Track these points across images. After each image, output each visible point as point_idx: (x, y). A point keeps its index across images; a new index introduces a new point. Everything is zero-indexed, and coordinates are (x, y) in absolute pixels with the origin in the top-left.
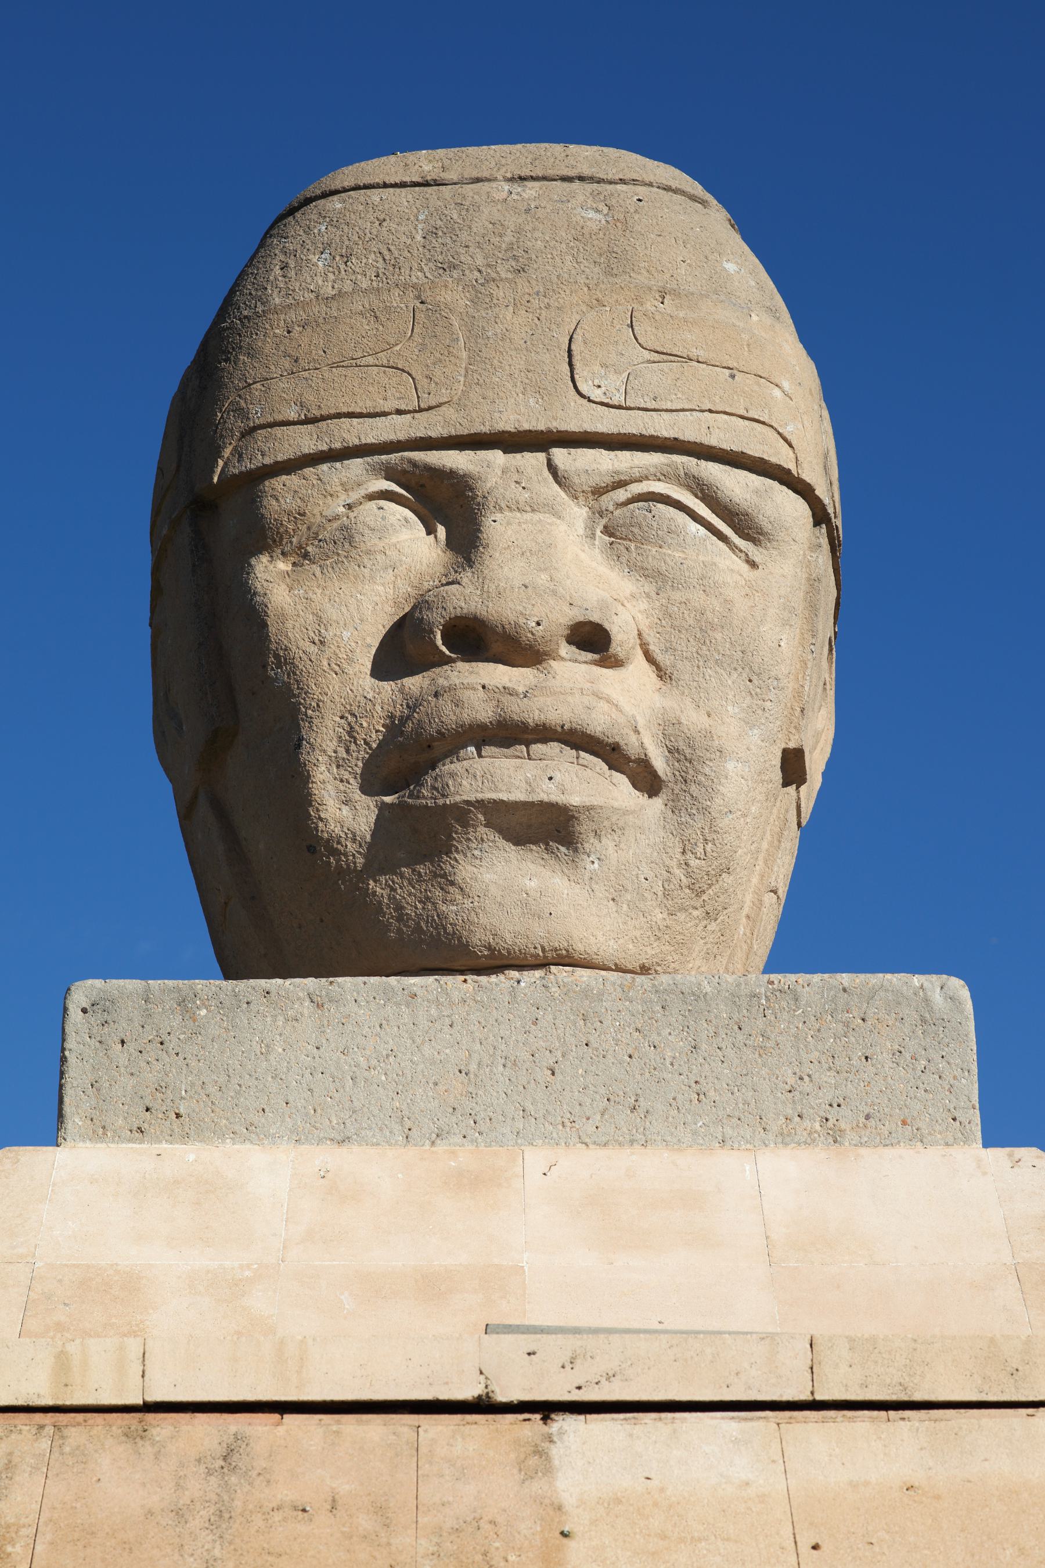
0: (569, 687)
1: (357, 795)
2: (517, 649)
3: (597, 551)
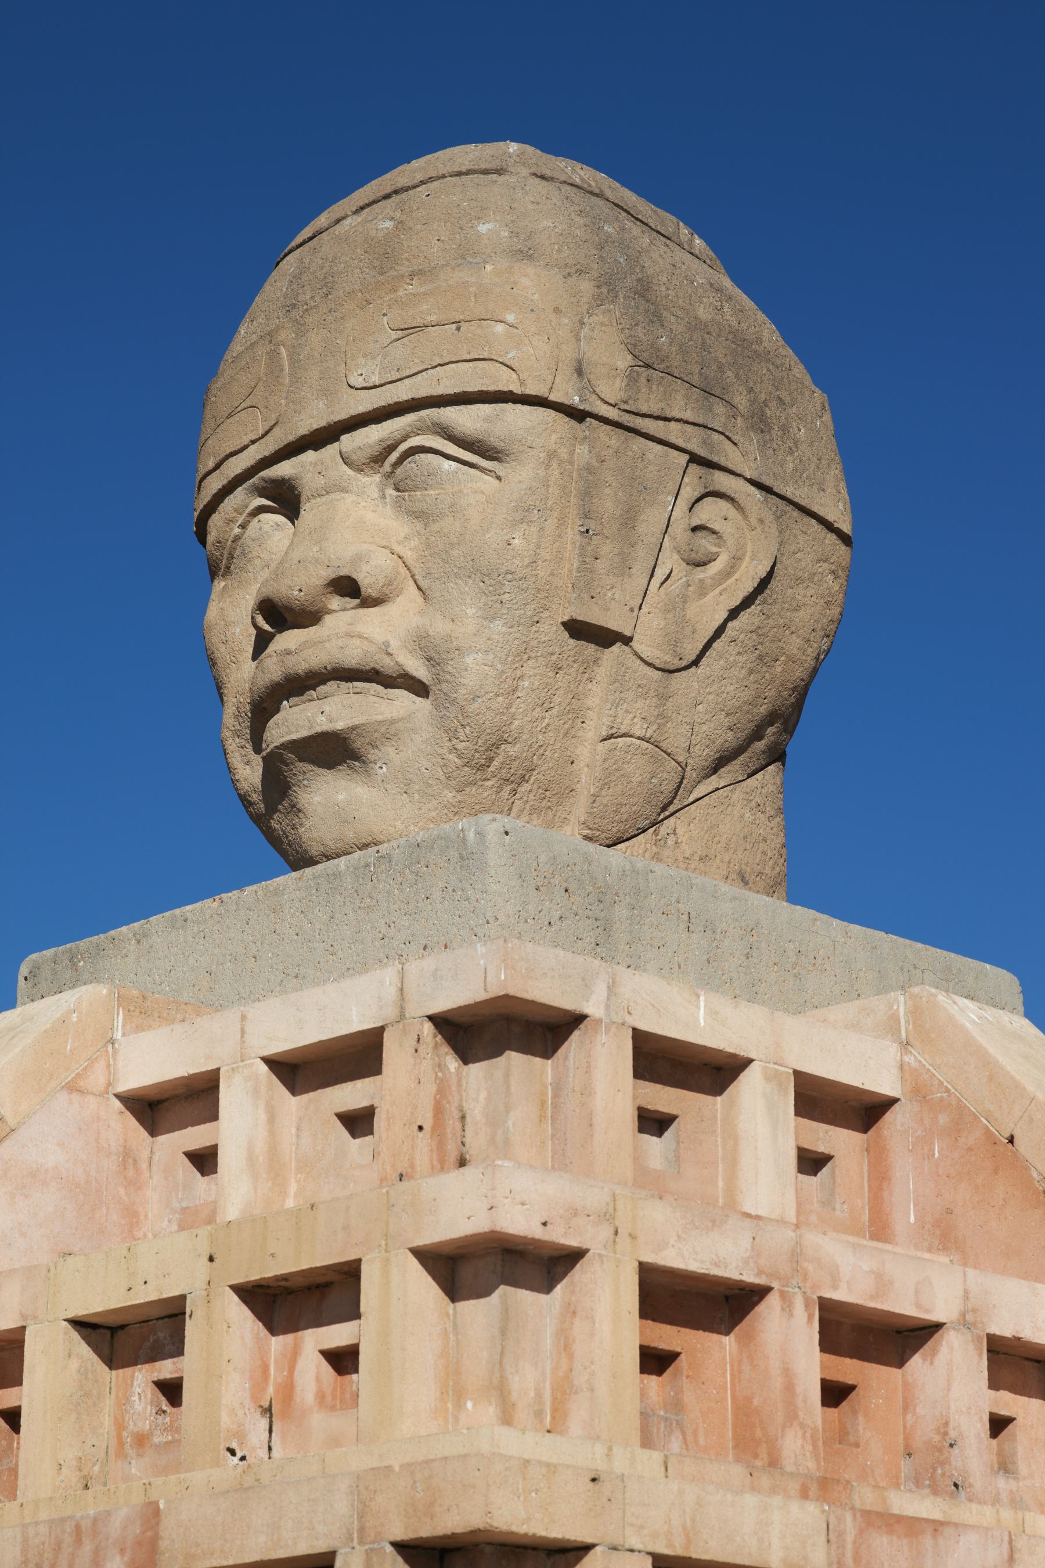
3: (389, 507)
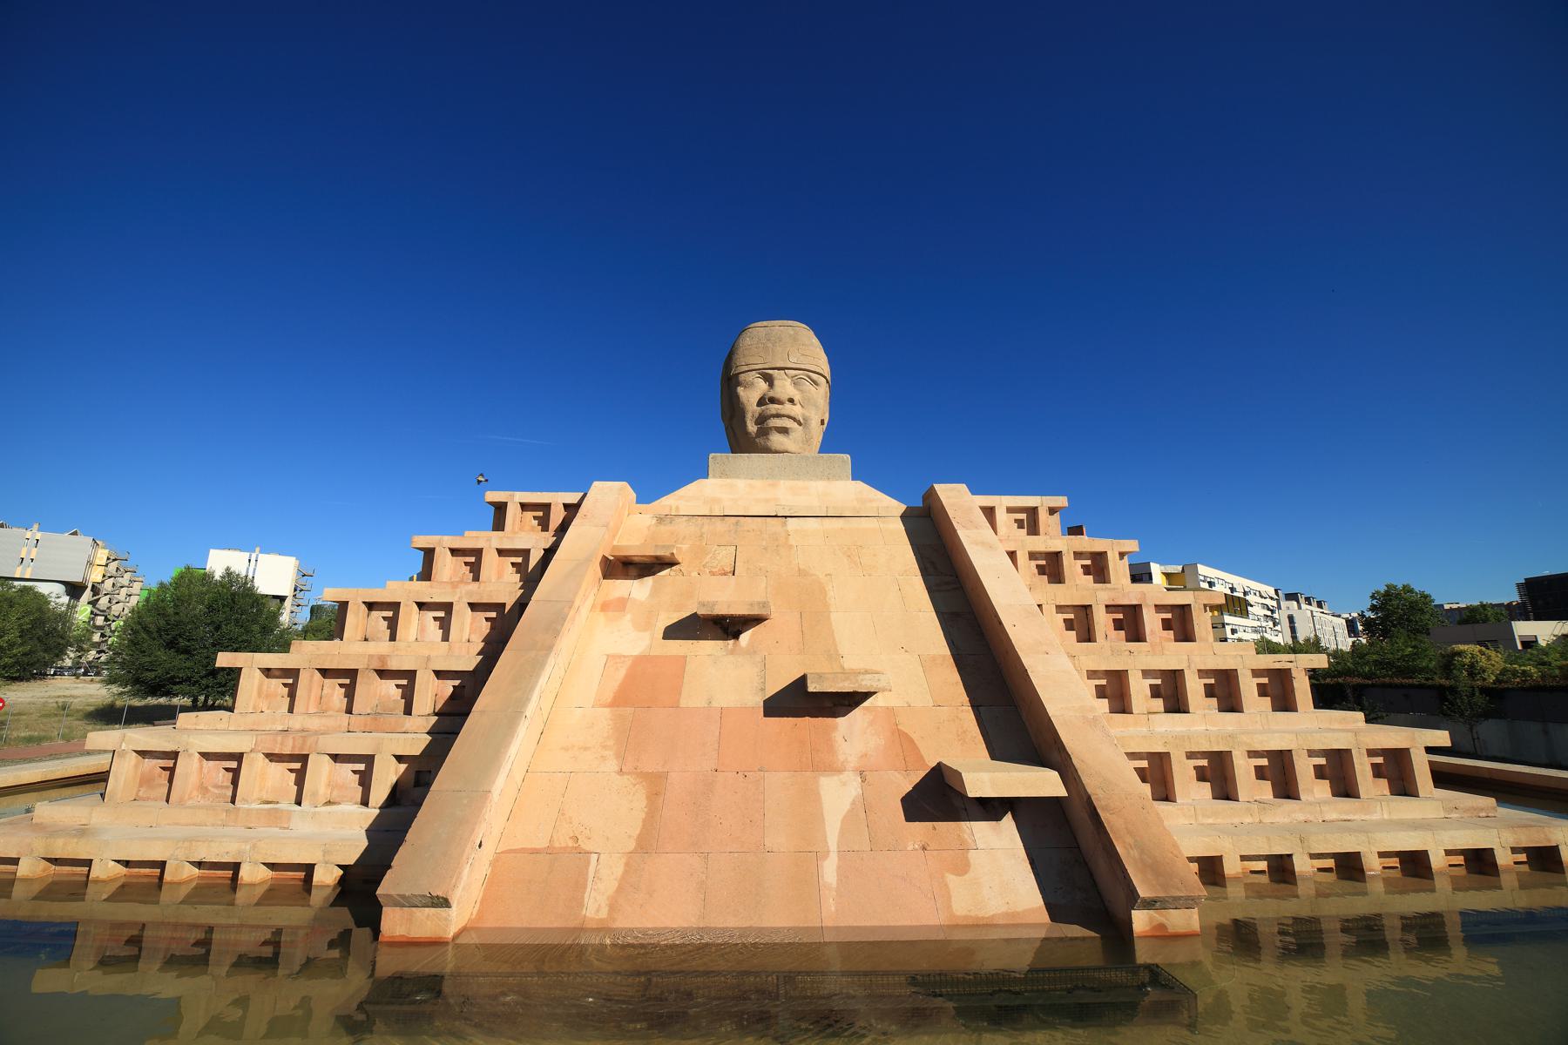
0: (787, 408)
2: (779, 402)
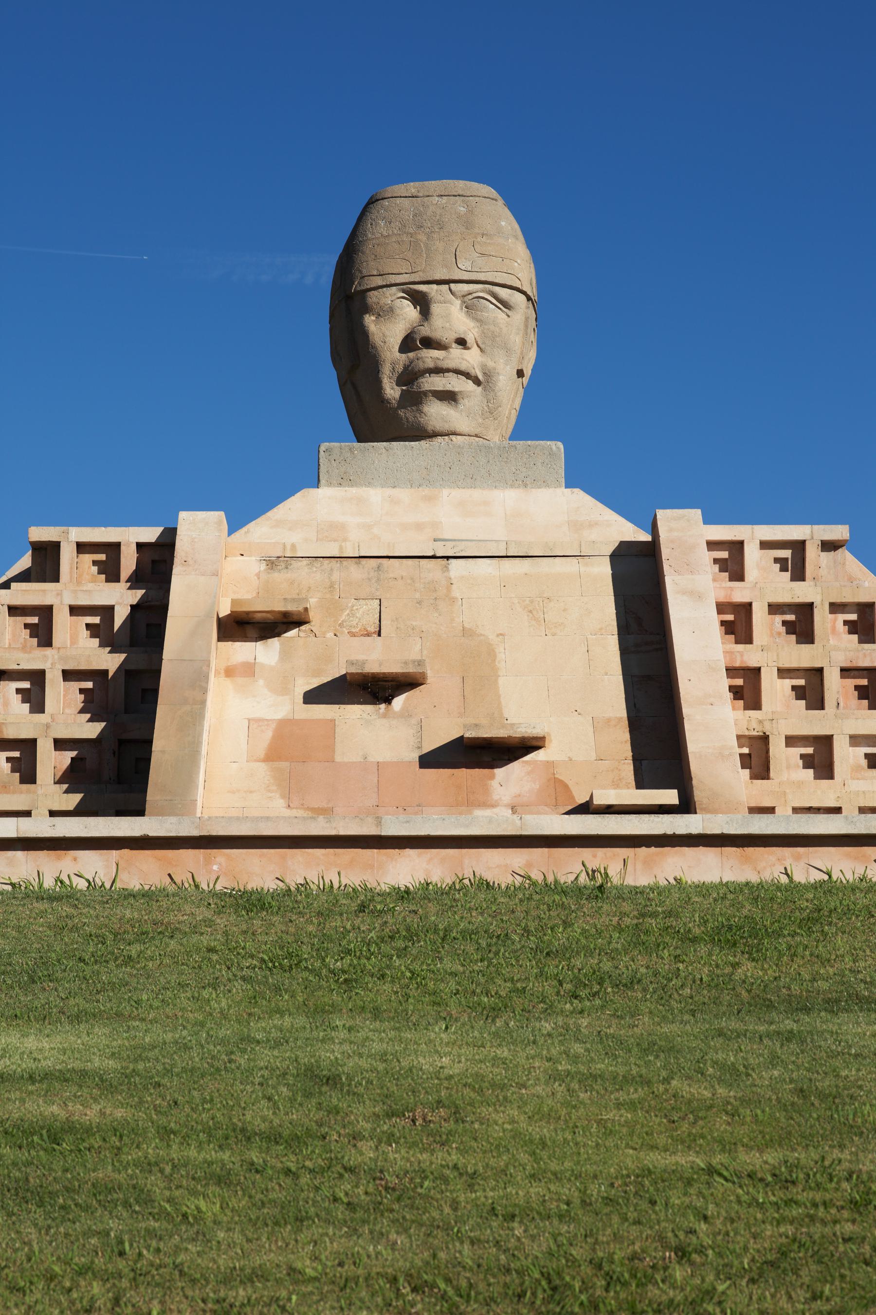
0: (456, 357)
1: (395, 387)
